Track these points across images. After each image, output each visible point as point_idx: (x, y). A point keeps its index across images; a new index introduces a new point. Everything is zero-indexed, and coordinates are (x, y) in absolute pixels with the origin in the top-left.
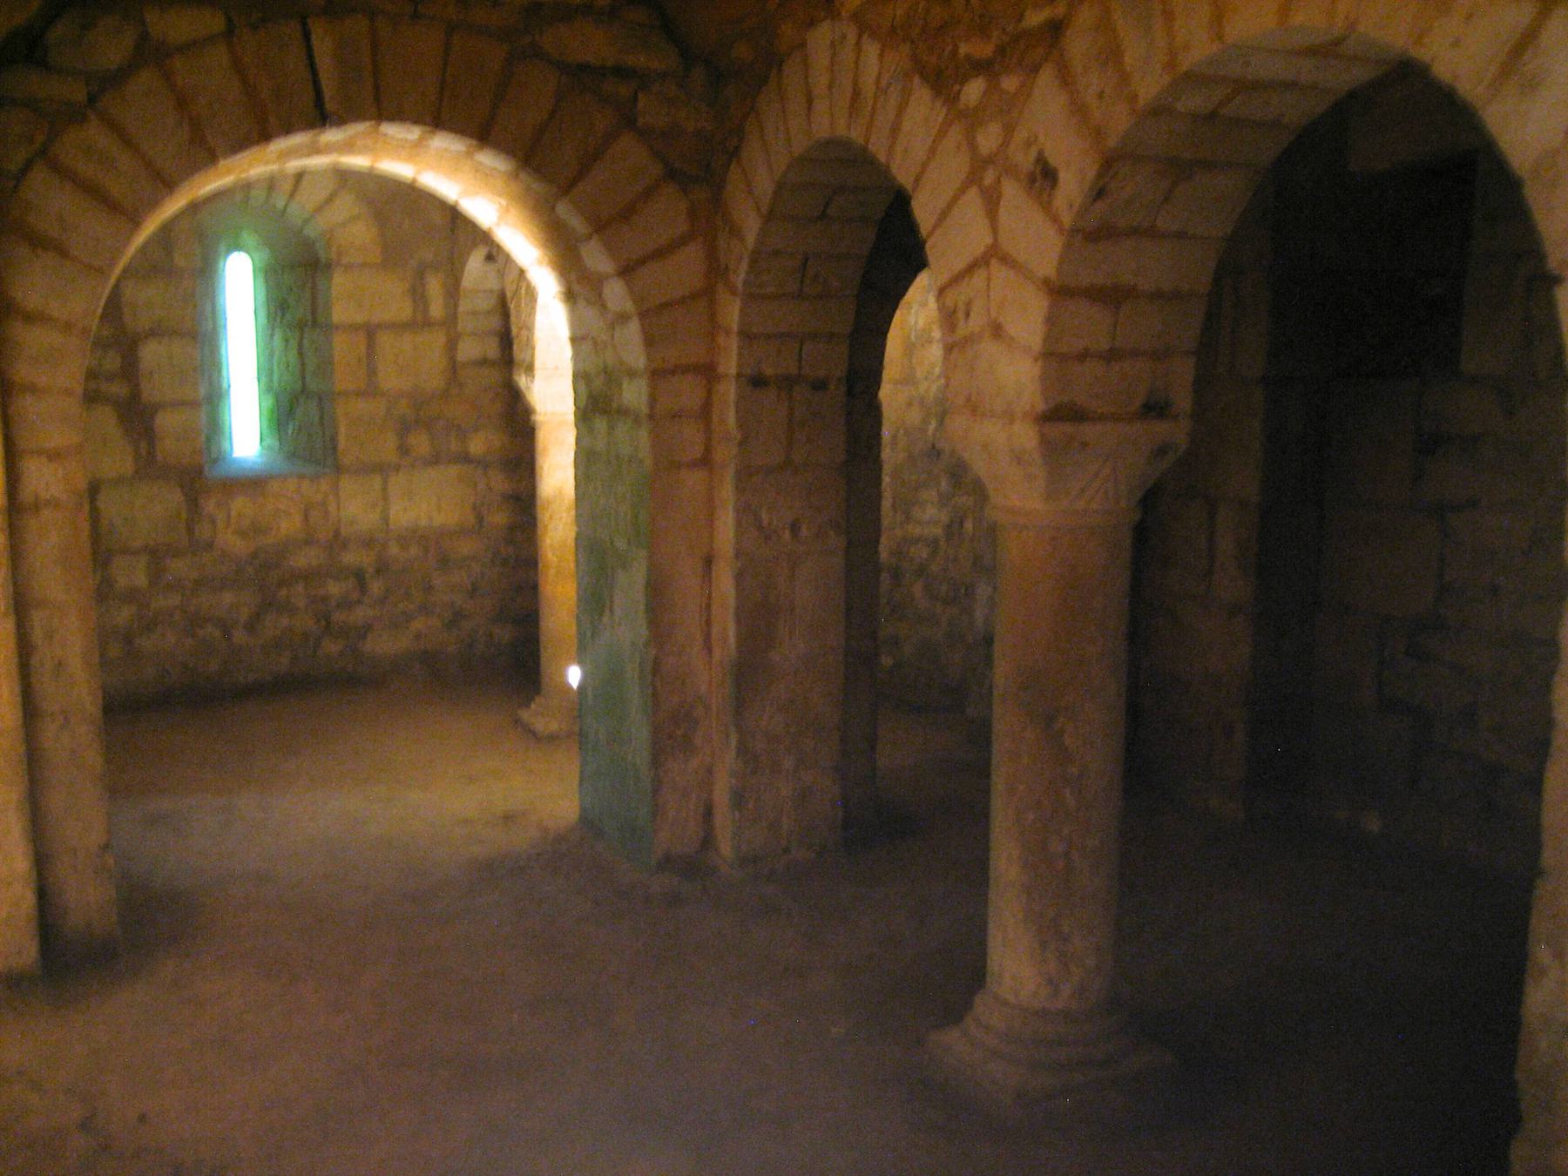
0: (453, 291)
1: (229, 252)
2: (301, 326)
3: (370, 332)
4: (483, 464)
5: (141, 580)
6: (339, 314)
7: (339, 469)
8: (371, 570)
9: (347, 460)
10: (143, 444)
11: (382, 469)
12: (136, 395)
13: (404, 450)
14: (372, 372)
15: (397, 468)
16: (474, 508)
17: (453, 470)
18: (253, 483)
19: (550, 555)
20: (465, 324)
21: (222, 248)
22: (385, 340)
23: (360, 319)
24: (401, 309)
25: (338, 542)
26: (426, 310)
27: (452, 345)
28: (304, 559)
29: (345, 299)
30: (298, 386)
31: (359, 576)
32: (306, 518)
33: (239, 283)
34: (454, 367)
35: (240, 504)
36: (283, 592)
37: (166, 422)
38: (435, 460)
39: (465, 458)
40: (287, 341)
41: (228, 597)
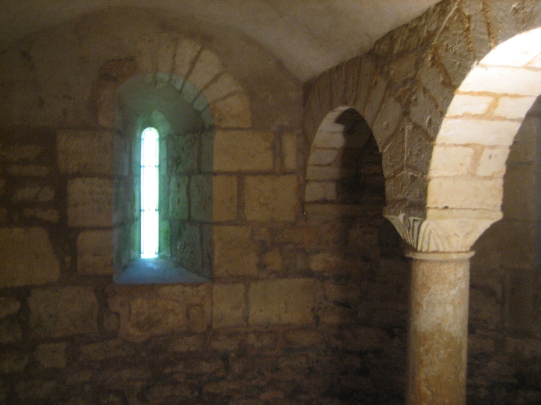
0: (306, 146)
1: (144, 127)
2: (189, 174)
3: (241, 176)
4: (320, 277)
5: (60, 361)
6: (219, 162)
7: (213, 279)
8: (233, 355)
9: (220, 272)
10: (68, 259)
11: (245, 279)
12: (64, 218)
13: (262, 266)
14: (241, 207)
15: (256, 279)
16: (313, 310)
17: (300, 281)
18: (149, 286)
19: (424, 388)
20: (311, 172)
21: (139, 122)
22: (250, 181)
23: (233, 167)
24: (264, 161)
25: (211, 332)
26: (282, 162)
27: (301, 188)
28: (183, 346)
29: (228, 152)
30: (185, 216)
31: (225, 358)
32: (188, 315)
33: (150, 145)
34: (302, 203)
35: (139, 303)
36: (168, 370)
37: (87, 241)
38: (285, 274)
39: (308, 273)
40: (179, 185)
41: (127, 374)
